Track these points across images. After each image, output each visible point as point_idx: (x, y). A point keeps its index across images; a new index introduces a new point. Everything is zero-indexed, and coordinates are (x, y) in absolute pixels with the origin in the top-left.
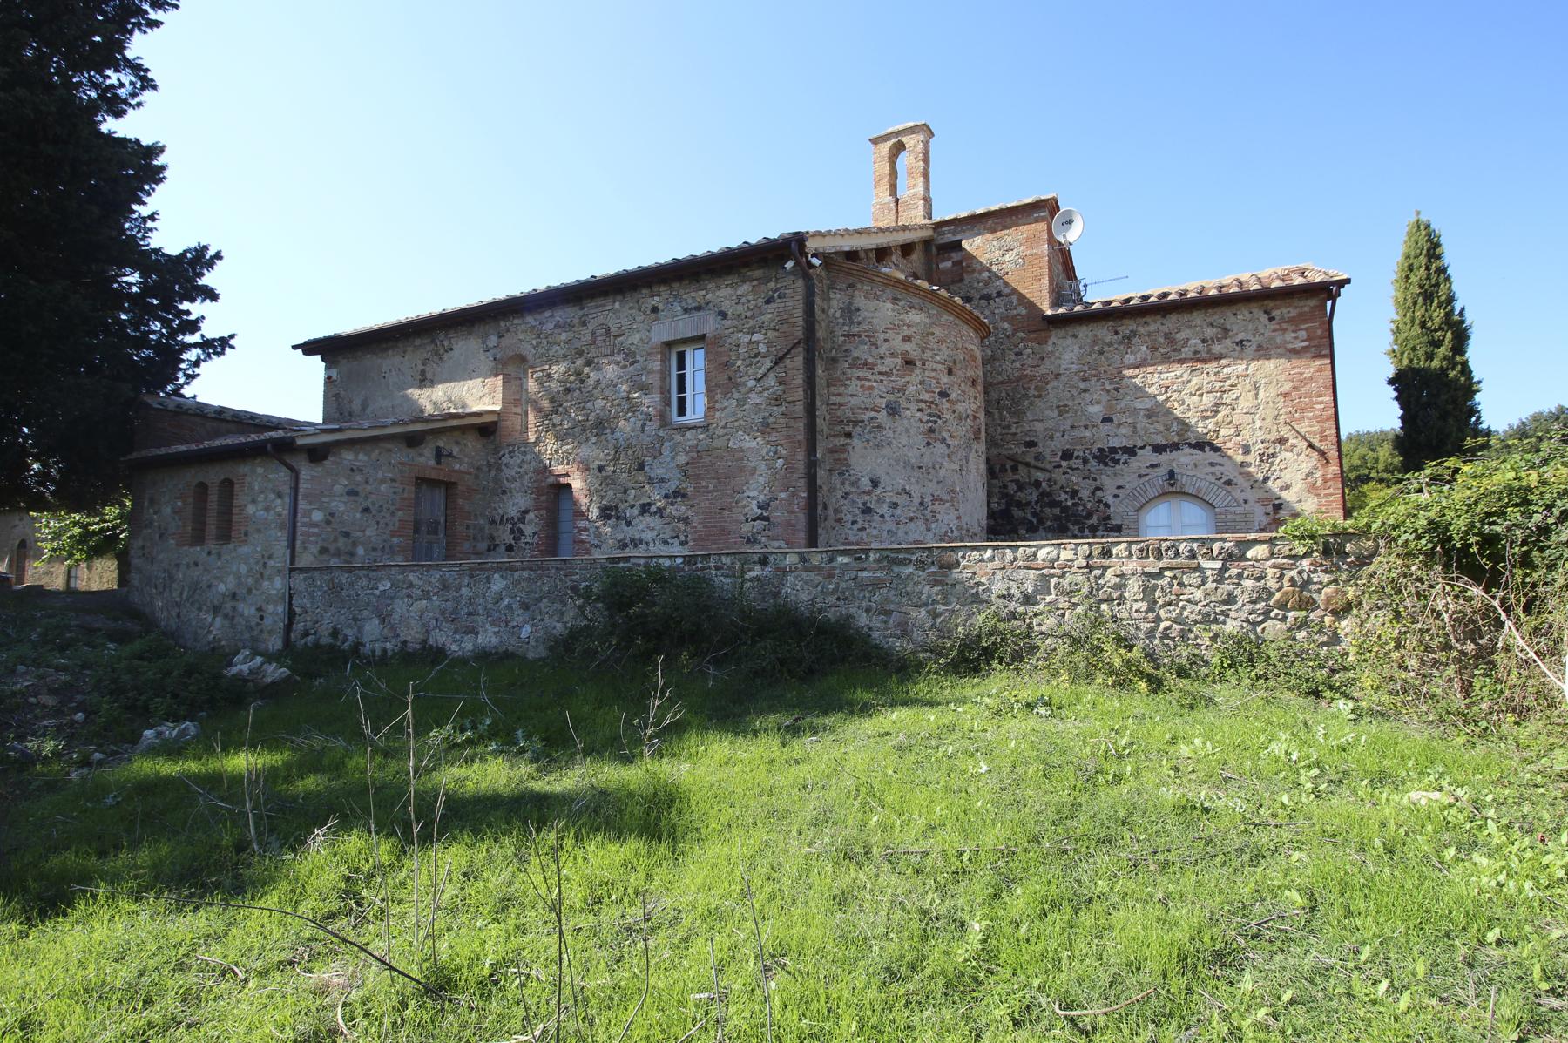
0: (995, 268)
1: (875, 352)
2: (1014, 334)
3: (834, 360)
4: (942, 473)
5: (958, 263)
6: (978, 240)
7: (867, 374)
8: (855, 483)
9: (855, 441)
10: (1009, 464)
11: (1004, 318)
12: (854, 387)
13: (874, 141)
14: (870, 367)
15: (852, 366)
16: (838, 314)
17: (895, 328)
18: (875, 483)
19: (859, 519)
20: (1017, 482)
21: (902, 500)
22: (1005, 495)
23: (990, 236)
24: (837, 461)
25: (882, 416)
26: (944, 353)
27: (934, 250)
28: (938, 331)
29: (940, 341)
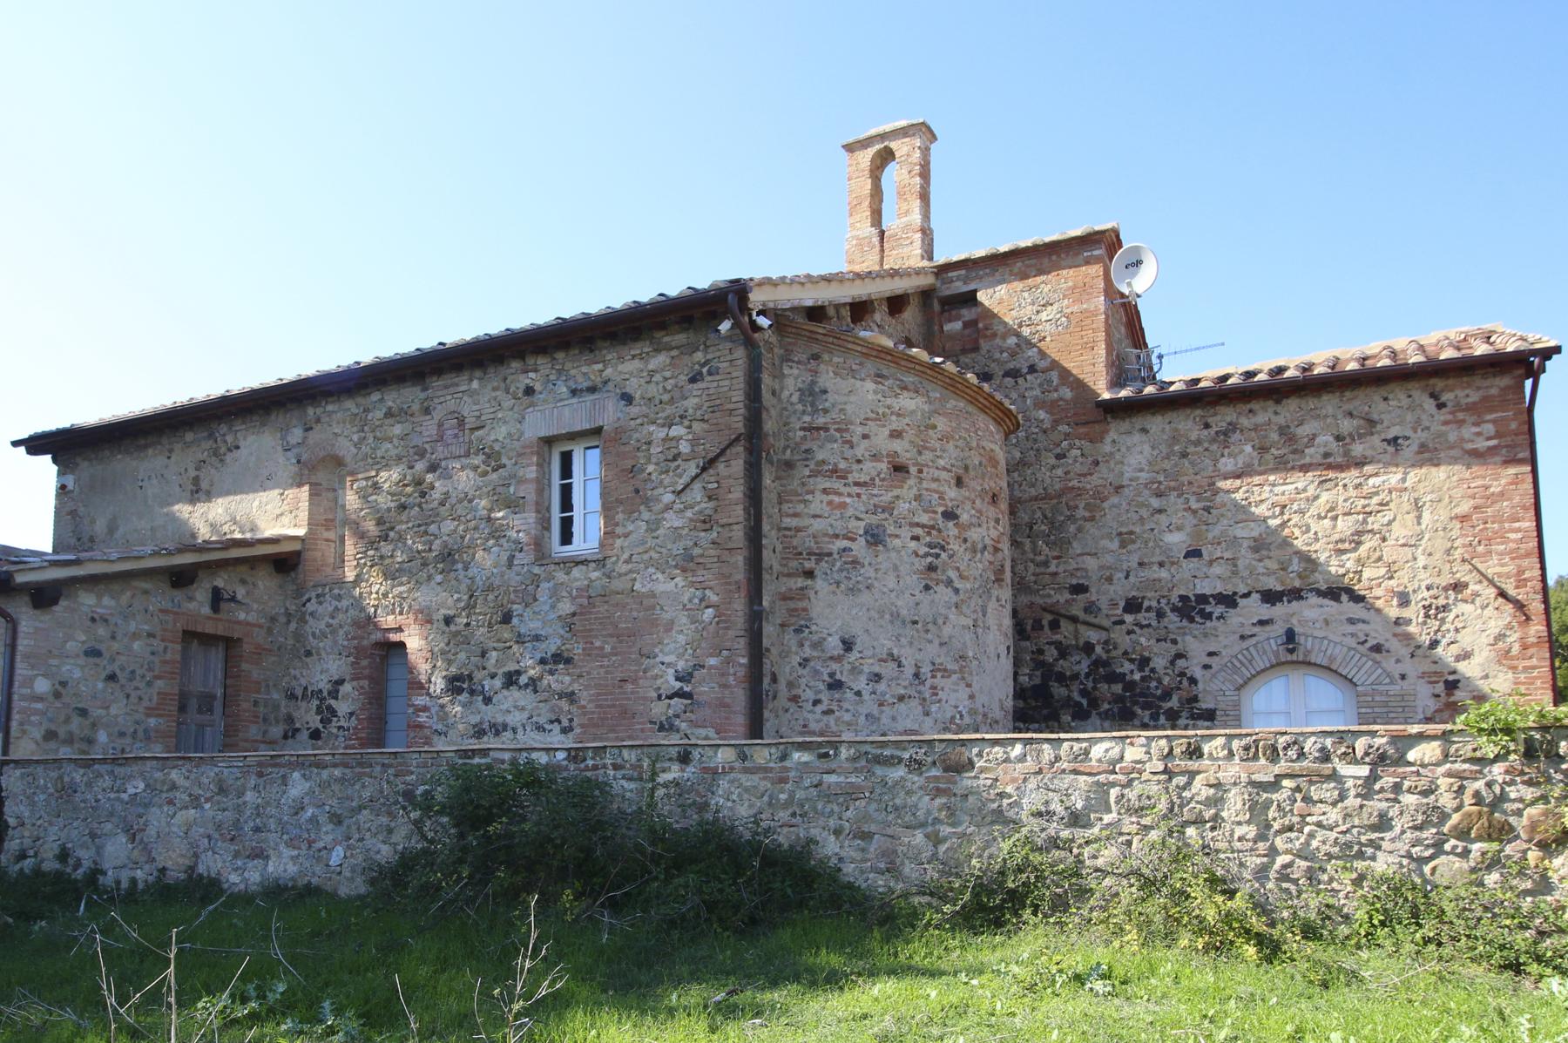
0: (1026, 331)
1: (849, 453)
2: (1054, 428)
3: (789, 465)
4: (947, 631)
6: (1002, 290)
7: (837, 485)
8: (816, 645)
9: (819, 583)
11: (1039, 404)
12: (818, 503)
13: (850, 148)
14: (835, 472)
16: (795, 398)
17: (879, 418)
18: (848, 645)
19: (824, 697)
21: (888, 669)
24: (792, 612)
25: (859, 548)
27: (937, 306)
28: (942, 423)
29: (945, 438)
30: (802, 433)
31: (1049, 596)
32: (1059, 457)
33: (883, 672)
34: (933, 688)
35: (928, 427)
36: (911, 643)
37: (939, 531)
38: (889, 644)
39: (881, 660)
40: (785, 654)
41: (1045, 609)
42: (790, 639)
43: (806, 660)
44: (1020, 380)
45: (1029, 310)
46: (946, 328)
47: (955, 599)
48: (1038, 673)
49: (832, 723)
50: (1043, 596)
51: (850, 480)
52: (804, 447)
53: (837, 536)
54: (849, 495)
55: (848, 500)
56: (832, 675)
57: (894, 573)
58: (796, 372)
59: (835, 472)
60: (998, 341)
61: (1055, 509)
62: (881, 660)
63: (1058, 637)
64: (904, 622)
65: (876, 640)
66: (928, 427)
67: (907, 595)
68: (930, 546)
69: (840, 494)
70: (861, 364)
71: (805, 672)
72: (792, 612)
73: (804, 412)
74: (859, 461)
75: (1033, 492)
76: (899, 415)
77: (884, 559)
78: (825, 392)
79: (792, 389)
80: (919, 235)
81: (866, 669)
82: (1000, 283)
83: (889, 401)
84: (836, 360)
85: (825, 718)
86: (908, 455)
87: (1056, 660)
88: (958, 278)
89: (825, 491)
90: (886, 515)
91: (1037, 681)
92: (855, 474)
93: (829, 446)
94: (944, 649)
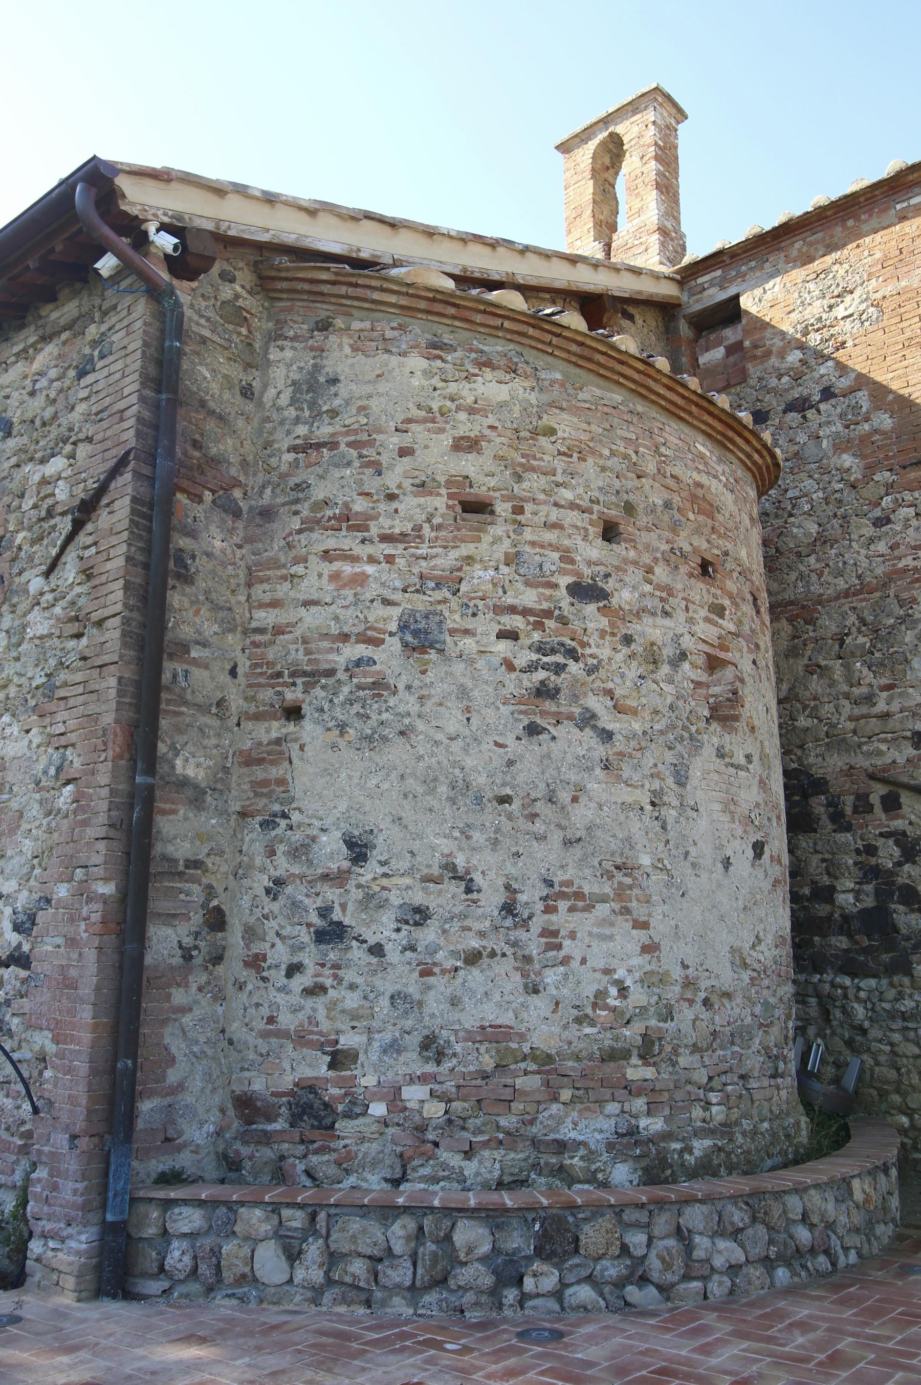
0: (814, 339)
1: (372, 484)
2: (868, 478)
3: (267, 514)
4: (581, 815)
5: (735, 349)
6: (775, 287)
7: (347, 541)
8: (300, 852)
9: (309, 729)
10: (878, 791)
11: (840, 446)
12: (315, 579)
13: (565, 148)
14: (348, 520)
15: (309, 526)
16: (284, 400)
18: (358, 850)
20: (899, 837)
21: (445, 898)
22: (871, 873)
23: (798, 274)
24: (260, 787)
25: (389, 657)
26: (591, 480)
27: (684, 329)
28: (567, 426)
29: (575, 452)
30: (291, 457)
31: (879, 753)
32: (879, 523)
33: (432, 903)
34: (549, 933)
36: (495, 843)
37: (563, 621)
38: (445, 845)
40: (239, 872)
41: (872, 777)
43: (279, 882)
44: (810, 414)
45: (817, 308)
46: (702, 360)
47: (600, 751)
48: (869, 888)
50: (869, 754)
51: (374, 531)
52: (293, 481)
53: (345, 637)
54: (372, 560)
55: (370, 569)
56: (324, 912)
58: (288, 354)
59: (348, 520)
60: (774, 361)
61: (879, 608)
63: (898, 824)
64: (479, 800)
67: (487, 745)
68: (540, 649)
69: (355, 559)
70: (401, 327)
71: (275, 907)
72: (260, 787)
73: (297, 421)
74: (391, 497)
75: (841, 584)
76: (471, 411)
77: (439, 677)
78: (334, 381)
79: (280, 386)
80: (656, 236)
83: (453, 388)
84: (356, 325)
85: (309, 1003)
86: (492, 482)
87: (899, 864)
88: (712, 284)
89: (326, 555)
90: (445, 593)
91: (869, 902)
92: (385, 522)
93: (337, 473)
94: (577, 851)
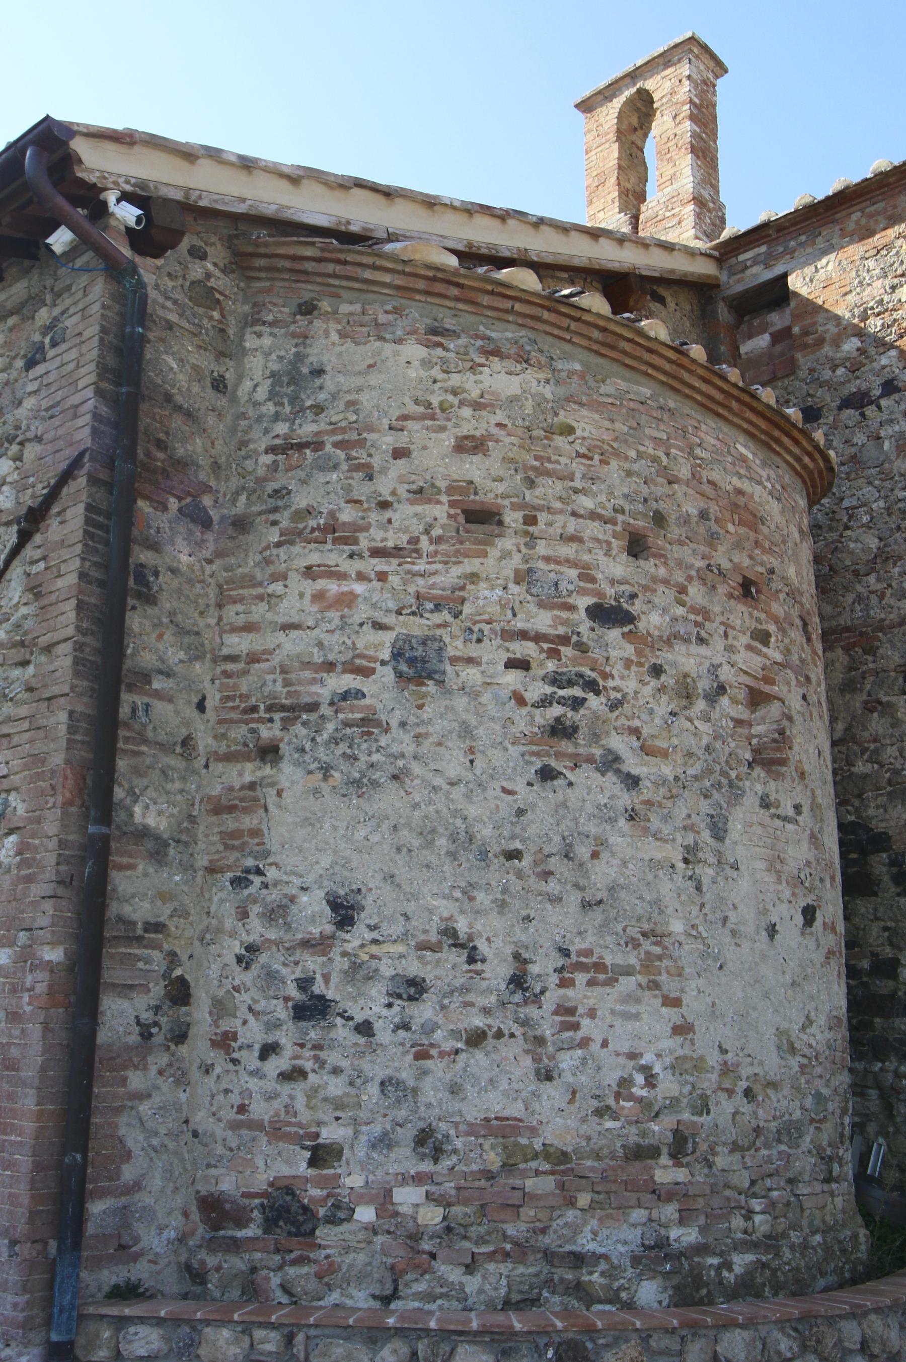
0: (874, 325)
1: (361, 490)
4: (602, 874)
6: (828, 265)
7: (333, 556)
8: (277, 913)
9: (288, 773)
12: (295, 599)
13: (586, 106)
14: (334, 532)
15: (289, 538)
16: (262, 393)
17: (432, 415)
19: (286, 1037)
21: (443, 970)
23: (855, 250)
24: (231, 840)
25: (380, 690)
26: (616, 485)
27: (723, 313)
29: (597, 453)
30: (268, 459)
33: (429, 974)
34: (565, 1009)
35: (550, 431)
37: (582, 648)
38: (445, 908)
39: (423, 946)
42: (222, 899)
43: (252, 949)
44: (870, 411)
46: (743, 349)
47: (625, 799)
49: (300, 1103)
51: (364, 544)
53: (330, 666)
54: (361, 577)
55: (359, 588)
56: (304, 984)
57: (468, 744)
58: (267, 341)
59: (334, 532)
60: (827, 350)
62: (423, 946)
64: (483, 855)
65: (413, 898)
66: (550, 431)
67: (494, 790)
68: (555, 680)
69: (342, 576)
70: (396, 311)
71: (247, 978)
72: (231, 840)
73: (276, 417)
76: (477, 406)
77: (438, 711)
78: (319, 372)
79: (258, 376)
80: (691, 207)
81: (386, 969)
82: (825, 252)
83: (455, 380)
84: (345, 308)
85: (286, 1089)
86: (501, 488)
88: (755, 261)
89: (309, 572)
90: (445, 616)
92: (376, 534)
93: (321, 478)
94: (598, 915)
